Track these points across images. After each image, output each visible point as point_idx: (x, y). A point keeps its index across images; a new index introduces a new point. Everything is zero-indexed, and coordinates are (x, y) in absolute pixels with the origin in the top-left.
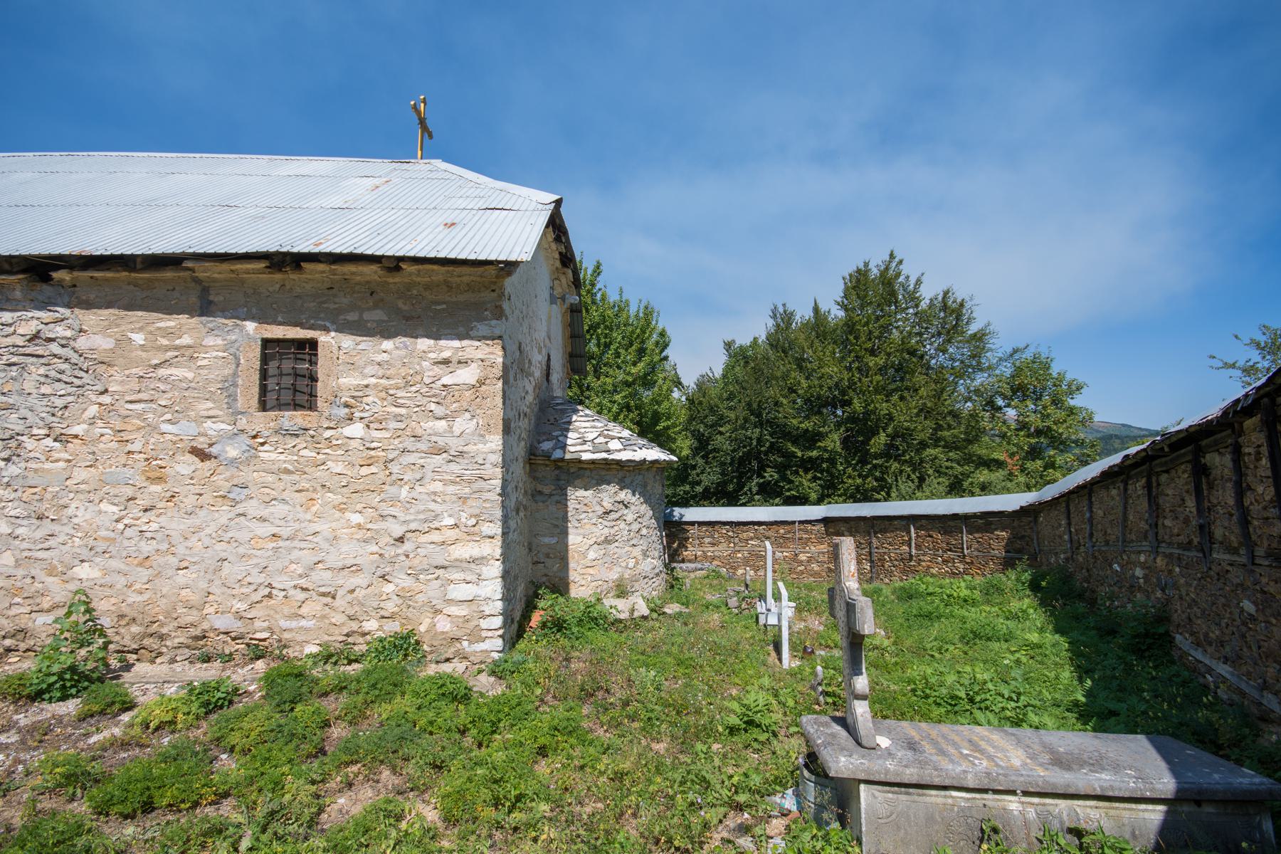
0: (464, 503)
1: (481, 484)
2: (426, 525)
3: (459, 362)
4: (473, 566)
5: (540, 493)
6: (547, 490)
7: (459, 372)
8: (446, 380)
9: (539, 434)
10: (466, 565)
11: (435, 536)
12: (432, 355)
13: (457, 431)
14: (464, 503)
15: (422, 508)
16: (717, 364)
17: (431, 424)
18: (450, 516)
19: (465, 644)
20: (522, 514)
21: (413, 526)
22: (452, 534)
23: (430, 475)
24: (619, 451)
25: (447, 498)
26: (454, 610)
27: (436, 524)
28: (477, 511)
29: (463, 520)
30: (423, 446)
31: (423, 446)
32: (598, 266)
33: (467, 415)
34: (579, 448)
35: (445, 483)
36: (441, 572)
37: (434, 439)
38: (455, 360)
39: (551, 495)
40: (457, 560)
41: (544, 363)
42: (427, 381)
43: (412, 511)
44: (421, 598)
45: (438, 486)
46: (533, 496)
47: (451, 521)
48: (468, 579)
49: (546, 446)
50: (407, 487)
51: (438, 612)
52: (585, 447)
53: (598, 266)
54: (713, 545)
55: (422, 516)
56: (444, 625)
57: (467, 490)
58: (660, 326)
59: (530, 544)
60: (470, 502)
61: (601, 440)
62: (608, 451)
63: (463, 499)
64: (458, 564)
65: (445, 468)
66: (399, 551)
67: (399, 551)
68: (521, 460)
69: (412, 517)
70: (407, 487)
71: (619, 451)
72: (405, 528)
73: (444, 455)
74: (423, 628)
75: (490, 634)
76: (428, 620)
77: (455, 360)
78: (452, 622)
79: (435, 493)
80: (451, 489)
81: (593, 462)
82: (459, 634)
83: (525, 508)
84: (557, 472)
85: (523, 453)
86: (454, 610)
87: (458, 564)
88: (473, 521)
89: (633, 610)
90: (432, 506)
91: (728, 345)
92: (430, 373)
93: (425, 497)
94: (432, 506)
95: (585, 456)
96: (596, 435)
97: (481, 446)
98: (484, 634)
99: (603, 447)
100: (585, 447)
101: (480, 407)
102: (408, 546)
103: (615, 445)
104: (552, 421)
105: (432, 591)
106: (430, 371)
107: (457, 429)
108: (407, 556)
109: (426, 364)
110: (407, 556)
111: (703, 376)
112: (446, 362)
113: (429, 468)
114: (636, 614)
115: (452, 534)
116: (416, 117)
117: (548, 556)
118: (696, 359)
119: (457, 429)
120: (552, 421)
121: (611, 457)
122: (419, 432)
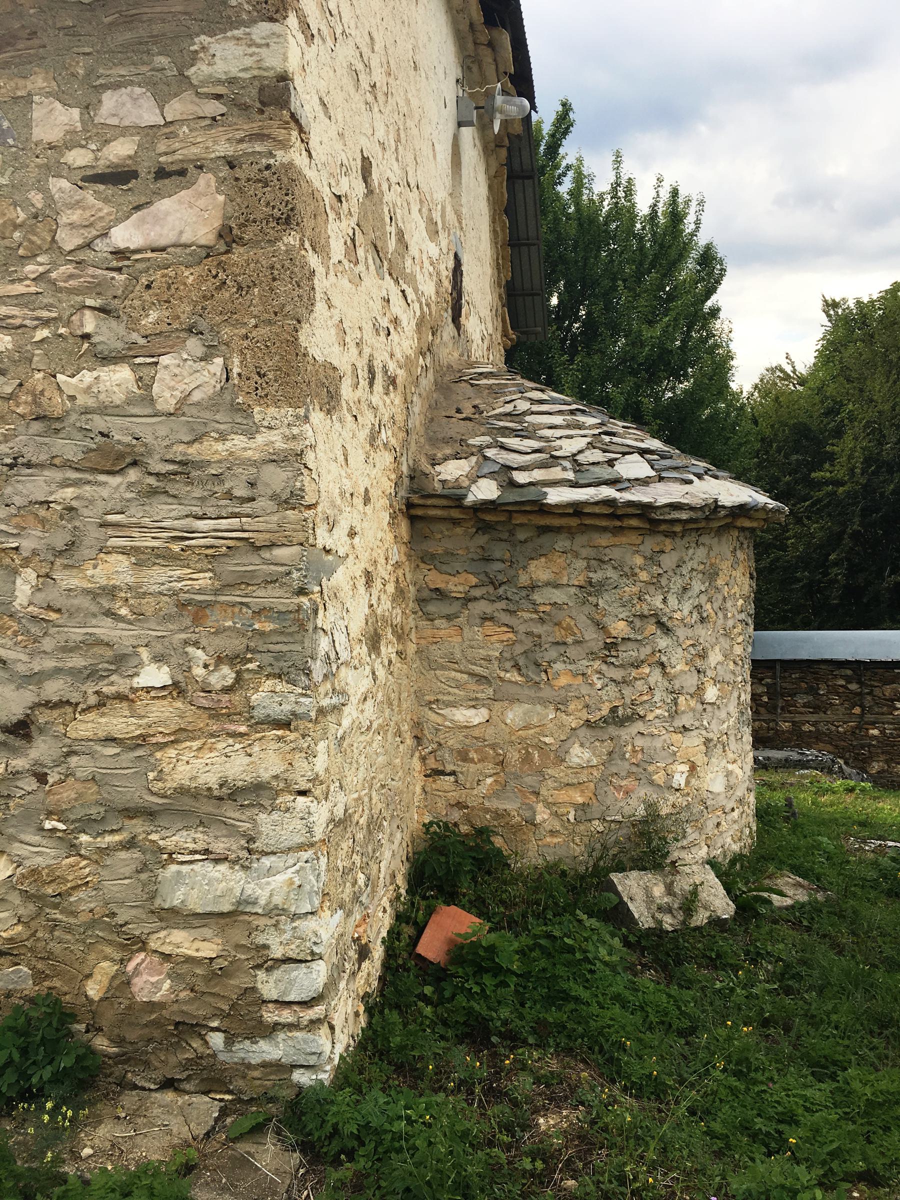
0: (197, 620)
1: (249, 563)
2: (90, 688)
3: (162, 174)
4: (230, 812)
5: (440, 594)
6: (456, 586)
7: (164, 205)
8: (125, 235)
9: (433, 441)
10: (207, 807)
11: (119, 722)
12: (78, 158)
13: (166, 399)
14: (197, 620)
15: (77, 633)
16: (804, 354)
17: (87, 377)
18: (159, 659)
19: (217, 1040)
20: (388, 650)
21: (53, 689)
22: (165, 713)
23: (94, 534)
24: (645, 482)
25: (148, 605)
26: (180, 941)
27: (119, 684)
28: (236, 644)
29: (199, 671)
30: (68, 448)
31: (68, 448)
32: (566, 107)
33: (194, 345)
34: (538, 475)
35: (142, 558)
36: (138, 826)
37: (99, 423)
38: (145, 168)
39: (468, 600)
40: (182, 791)
41: (446, 274)
42: (68, 240)
43: (48, 644)
44: (84, 901)
45: (116, 569)
46: (421, 601)
47: (155, 675)
48: (219, 847)
49: (453, 470)
50: (30, 574)
51: (141, 944)
52: (556, 473)
53: (566, 107)
54: (817, 708)
55: (77, 661)
56: (152, 984)
57: (204, 580)
58: (702, 240)
59: (417, 725)
60: (215, 618)
61: (597, 456)
62: (613, 482)
63: (193, 609)
64: (187, 803)
65: (136, 513)
66: (19, 763)
67: (19, 763)
68: (380, 503)
69: (50, 664)
70: (30, 574)
71: (645, 482)
72: (28, 696)
73: (133, 475)
74: (94, 990)
75: (286, 1016)
76: (106, 969)
77: (145, 168)
78: (173, 975)
79: (111, 592)
80: (158, 577)
81: (577, 509)
82: (198, 1011)
83: (401, 635)
84: (482, 540)
85: (388, 486)
86: (180, 941)
87: (187, 803)
88: (227, 675)
89: (181, 232)
90: (104, 629)
91: (830, 306)
92: (75, 216)
93: (85, 602)
94: (104, 629)
95: (556, 496)
96: (581, 443)
97: (238, 442)
98: (270, 1016)
99: (605, 473)
100: (556, 473)
101: (231, 315)
102: (42, 749)
103: (633, 467)
104: (468, 411)
105: (119, 878)
106: (78, 210)
107: (166, 395)
108: (42, 778)
109: (60, 186)
110: (42, 778)
111: (772, 370)
112: (118, 177)
113: (90, 515)
114: (700, 918)
115: (165, 713)
116: (311, 145)
117: (463, 756)
118: (768, 332)
119: (166, 395)
120: (468, 411)
121: (627, 496)
122: (56, 404)
